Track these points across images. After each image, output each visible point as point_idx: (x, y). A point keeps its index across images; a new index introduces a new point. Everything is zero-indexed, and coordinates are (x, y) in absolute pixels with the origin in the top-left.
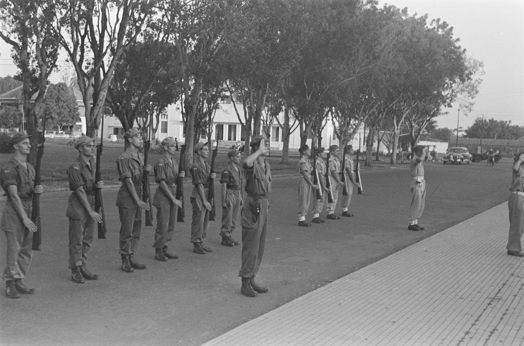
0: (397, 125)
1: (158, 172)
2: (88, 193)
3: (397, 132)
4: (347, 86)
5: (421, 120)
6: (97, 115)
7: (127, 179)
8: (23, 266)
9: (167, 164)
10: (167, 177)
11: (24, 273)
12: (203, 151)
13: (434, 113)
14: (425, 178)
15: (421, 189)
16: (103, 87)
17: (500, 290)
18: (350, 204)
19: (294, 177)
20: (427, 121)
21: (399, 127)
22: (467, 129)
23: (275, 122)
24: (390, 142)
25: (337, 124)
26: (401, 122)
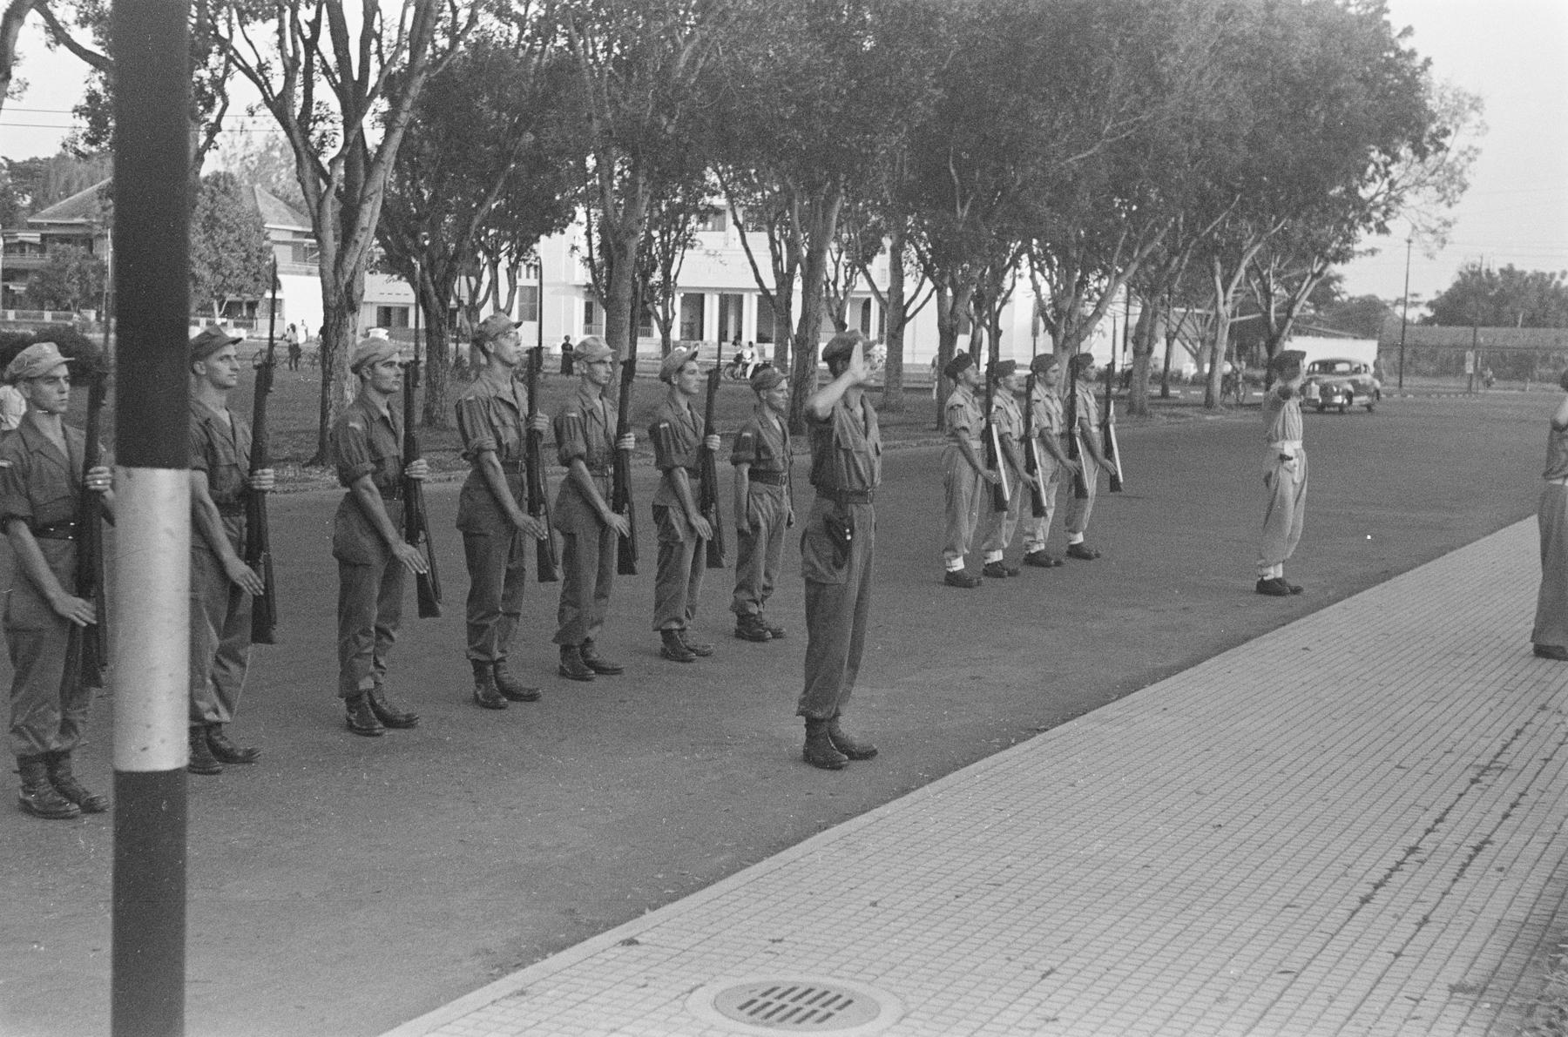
0: (1225, 290)
1: (566, 437)
2: (386, 491)
3: (1225, 310)
5: (1296, 272)
6: (354, 273)
7: (485, 455)
8: (226, 689)
9: (591, 412)
10: (589, 448)
11: (229, 708)
13: (1338, 252)
14: (1306, 446)
15: (1294, 476)
16: (370, 191)
17: (1505, 747)
20: (1314, 276)
21: (1230, 295)
22: (1433, 297)
23: (861, 285)
24: (1202, 341)
25: (1045, 289)
26: (1237, 280)
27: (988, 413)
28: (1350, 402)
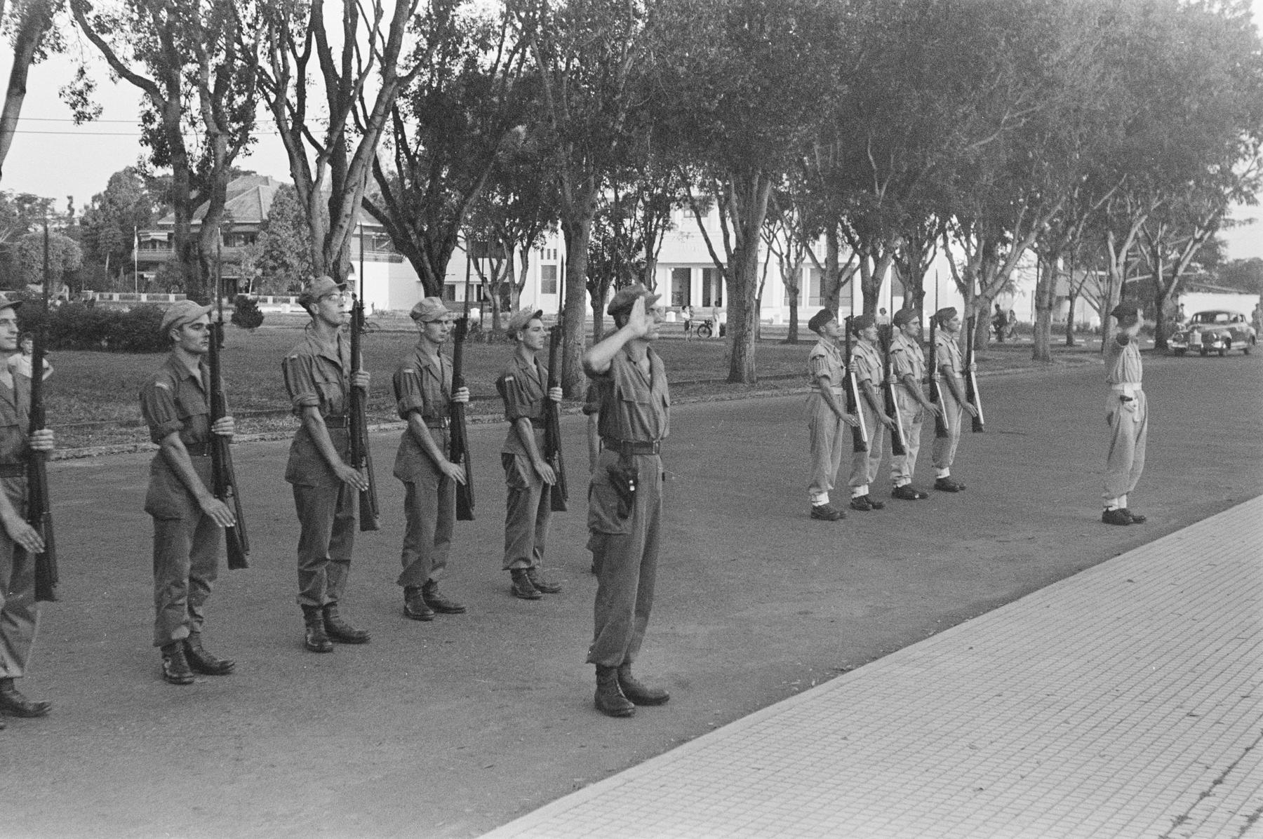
0: (1118, 254)
1: (403, 393)
3: (1118, 271)
4: (978, 159)
7: (308, 410)
9: (427, 368)
11: (20, 662)
12: (530, 332)
13: (1211, 222)
15: (1134, 416)
16: (351, 183)
18: (956, 458)
19: (801, 393)
27: (847, 361)
28: (1229, 347)
